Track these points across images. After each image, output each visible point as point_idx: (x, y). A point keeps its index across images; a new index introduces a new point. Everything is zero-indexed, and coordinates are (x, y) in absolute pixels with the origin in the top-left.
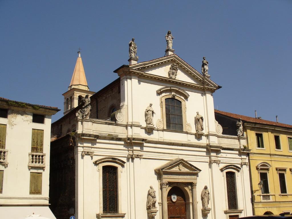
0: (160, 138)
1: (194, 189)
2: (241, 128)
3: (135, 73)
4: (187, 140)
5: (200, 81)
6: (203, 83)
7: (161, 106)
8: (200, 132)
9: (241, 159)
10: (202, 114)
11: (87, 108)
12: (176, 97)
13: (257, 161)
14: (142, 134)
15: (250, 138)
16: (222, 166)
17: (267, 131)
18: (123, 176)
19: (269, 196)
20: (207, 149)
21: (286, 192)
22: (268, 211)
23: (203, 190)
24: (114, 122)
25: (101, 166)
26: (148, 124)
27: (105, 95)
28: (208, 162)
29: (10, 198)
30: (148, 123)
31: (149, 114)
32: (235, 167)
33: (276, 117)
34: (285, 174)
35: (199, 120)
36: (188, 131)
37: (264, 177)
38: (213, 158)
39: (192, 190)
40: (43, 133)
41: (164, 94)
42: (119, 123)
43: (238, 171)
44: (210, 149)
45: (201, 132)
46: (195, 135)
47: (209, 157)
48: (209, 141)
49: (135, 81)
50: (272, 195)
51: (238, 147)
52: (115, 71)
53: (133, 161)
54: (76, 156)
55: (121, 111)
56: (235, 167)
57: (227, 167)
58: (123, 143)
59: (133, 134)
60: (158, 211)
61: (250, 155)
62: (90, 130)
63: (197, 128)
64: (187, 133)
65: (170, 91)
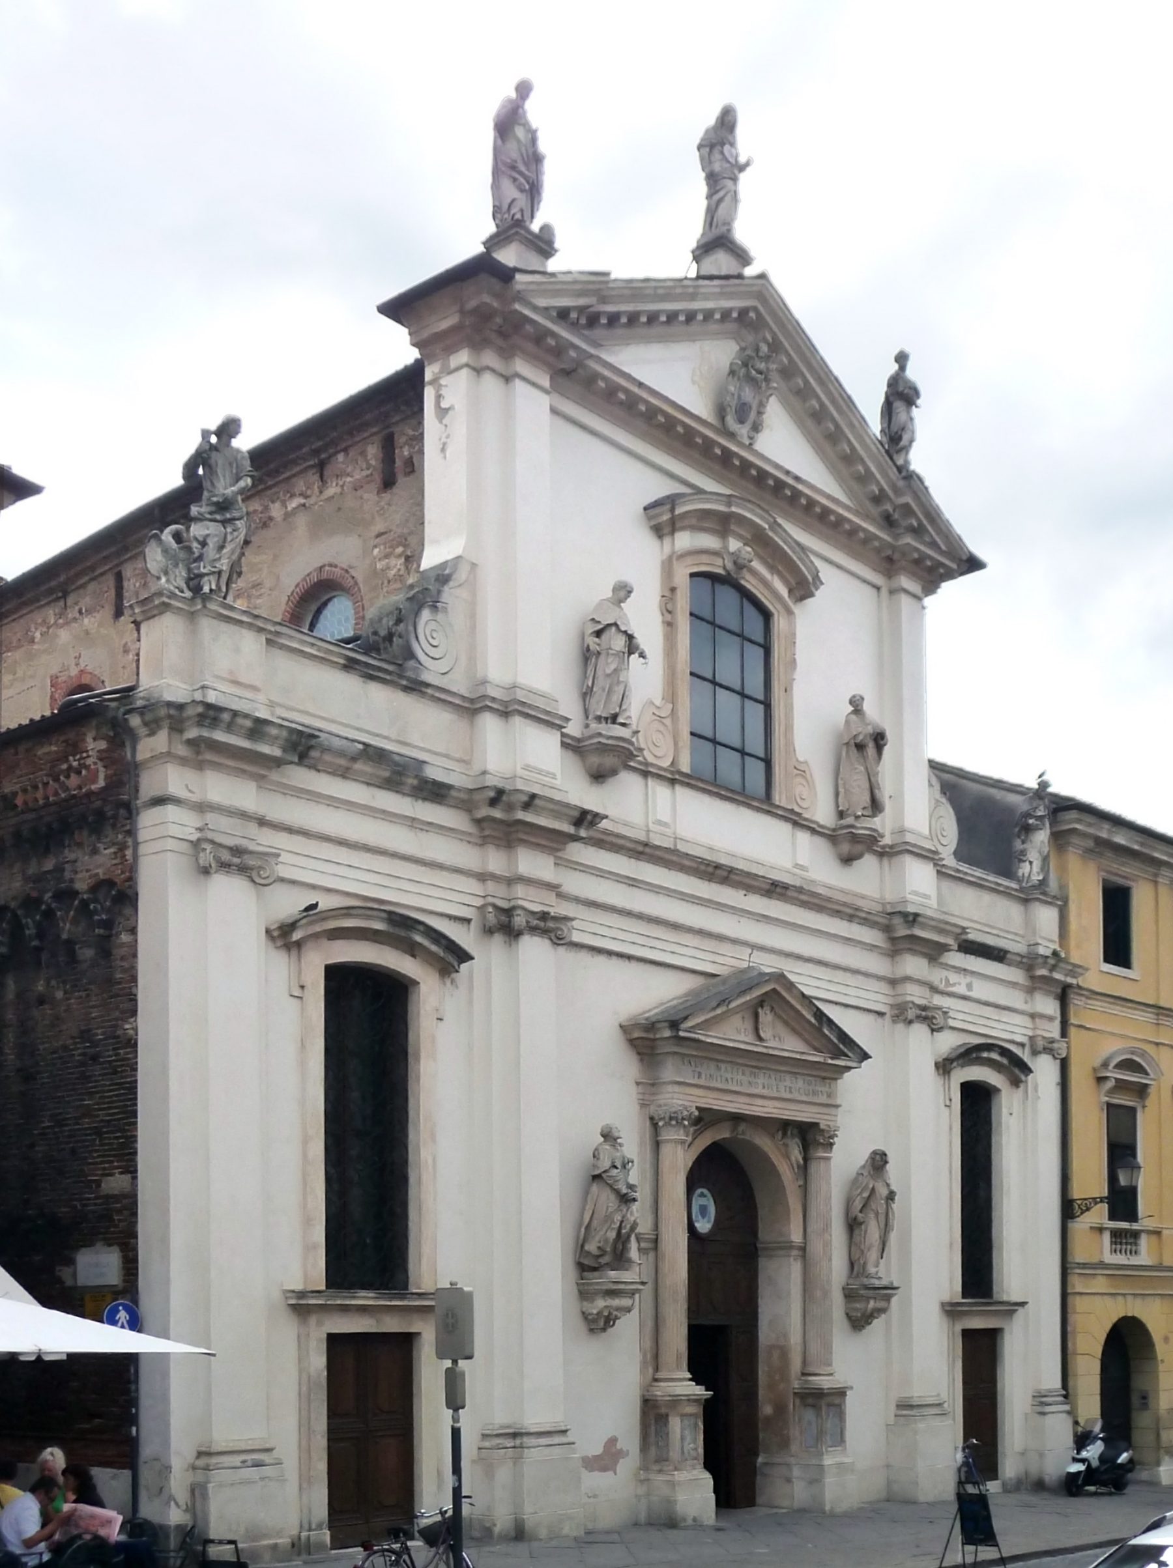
1: (813, 1167)
3: (540, 337)
4: (788, 865)
7: (668, 617)
8: (864, 826)
9: (1033, 1016)
11: (224, 522)
12: (748, 576)
13: (1104, 1036)
16: (948, 1042)
18: (448, 1041)
19: (1135, 1235)
21: (343, 983)
22: (1130, 1314)
23: (859, 1174)
26: (599, 719)
31: (600, 646)
32: (1005, 1061)
39: (804, 1170)
41: (684, 540)
43: (1016, 1083)
44: (903, 931)
49: (531, 404)
52: (396, 309)
60: (643, 1283)
61: (1076, 1001)
62: (249, 694)
64: (796, 820)
65: (722, 523)
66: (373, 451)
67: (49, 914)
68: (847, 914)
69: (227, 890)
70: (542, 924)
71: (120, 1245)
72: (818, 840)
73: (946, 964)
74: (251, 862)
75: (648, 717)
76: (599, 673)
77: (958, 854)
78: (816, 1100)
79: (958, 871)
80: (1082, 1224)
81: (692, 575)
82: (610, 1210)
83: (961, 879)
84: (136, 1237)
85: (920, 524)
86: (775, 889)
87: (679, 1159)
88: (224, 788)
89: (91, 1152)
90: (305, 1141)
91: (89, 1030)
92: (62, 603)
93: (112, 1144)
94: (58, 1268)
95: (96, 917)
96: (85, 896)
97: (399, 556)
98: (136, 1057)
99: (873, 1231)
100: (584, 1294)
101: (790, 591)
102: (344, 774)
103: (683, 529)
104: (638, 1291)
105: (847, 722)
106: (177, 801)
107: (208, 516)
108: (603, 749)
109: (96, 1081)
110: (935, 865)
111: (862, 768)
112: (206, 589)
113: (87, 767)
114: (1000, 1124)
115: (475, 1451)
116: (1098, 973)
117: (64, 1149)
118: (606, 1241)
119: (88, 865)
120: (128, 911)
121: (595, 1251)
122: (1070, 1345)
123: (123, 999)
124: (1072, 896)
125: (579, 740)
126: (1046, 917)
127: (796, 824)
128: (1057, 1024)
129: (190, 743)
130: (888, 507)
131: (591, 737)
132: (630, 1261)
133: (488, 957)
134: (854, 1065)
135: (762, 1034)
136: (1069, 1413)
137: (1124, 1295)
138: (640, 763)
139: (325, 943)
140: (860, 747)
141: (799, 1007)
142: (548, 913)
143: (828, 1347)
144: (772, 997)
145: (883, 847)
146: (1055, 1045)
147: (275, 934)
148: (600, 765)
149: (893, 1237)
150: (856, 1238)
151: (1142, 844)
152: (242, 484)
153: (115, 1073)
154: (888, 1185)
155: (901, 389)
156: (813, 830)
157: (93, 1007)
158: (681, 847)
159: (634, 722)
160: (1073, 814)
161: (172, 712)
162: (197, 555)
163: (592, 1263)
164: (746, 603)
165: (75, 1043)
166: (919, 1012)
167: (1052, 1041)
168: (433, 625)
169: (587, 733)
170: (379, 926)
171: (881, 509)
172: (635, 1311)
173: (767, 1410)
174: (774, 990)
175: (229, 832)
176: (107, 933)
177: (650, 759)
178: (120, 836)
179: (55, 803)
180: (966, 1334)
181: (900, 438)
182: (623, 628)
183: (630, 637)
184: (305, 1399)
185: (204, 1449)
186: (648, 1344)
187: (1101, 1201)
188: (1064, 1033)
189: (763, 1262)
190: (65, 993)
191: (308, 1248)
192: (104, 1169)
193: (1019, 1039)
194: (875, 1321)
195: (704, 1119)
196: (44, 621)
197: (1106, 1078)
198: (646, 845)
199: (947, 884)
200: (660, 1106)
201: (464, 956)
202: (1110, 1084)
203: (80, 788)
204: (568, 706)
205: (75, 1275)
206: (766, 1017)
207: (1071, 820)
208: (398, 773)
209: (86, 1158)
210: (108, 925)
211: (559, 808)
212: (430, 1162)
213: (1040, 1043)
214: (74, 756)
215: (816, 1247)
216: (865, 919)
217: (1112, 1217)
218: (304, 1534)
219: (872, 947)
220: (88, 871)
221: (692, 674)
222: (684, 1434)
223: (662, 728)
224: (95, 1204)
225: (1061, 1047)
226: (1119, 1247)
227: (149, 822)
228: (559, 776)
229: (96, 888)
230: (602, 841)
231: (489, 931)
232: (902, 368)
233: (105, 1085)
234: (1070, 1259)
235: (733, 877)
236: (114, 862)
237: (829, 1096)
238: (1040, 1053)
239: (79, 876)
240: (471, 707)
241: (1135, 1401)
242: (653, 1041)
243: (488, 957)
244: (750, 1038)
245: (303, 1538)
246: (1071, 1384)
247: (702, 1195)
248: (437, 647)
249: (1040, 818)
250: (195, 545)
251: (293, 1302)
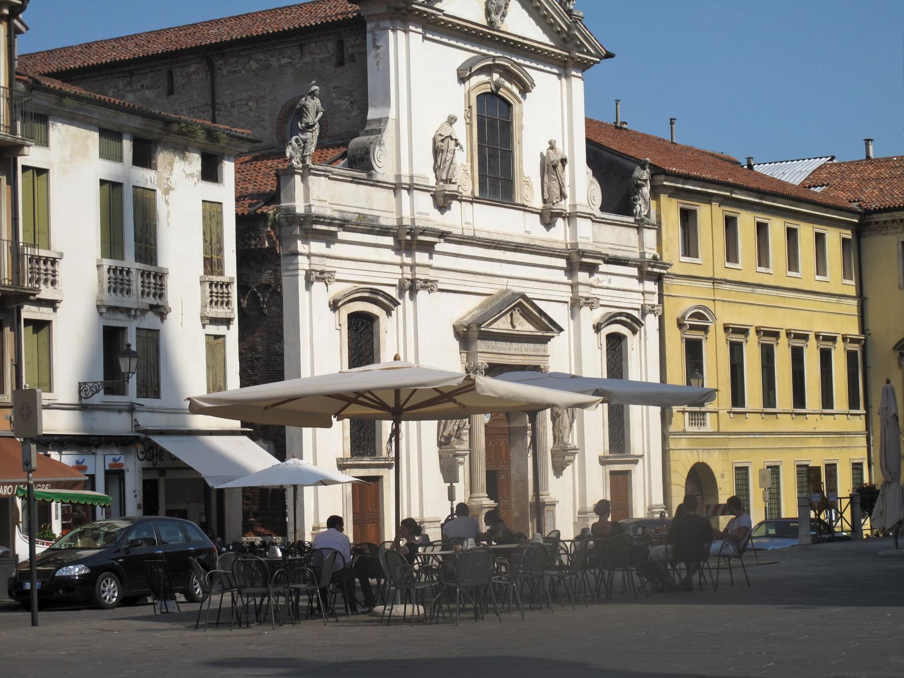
2: (646, 190)
4: (522, 232)
5: (558, 32)
6: (564, 40)
9: (643, 293)
10: (563, 149)
13: (684, 299)
14: (434, 219)
15: (667, 226)
16: (598, 314)
17: (708, 198)
19: (704, 413)
20: (568, 259)
21: (743, 405)
24: (364, 175)
26: (443, 180)
27: (261, 56)
28: (567, 302)
30: (444, 177)
32: (629, 321)
33: (672, 124)
35: (551, 167)
36: (526, 204)
37: (694, 351)
38: (583, 292)
40: (221, 212)
41: (475, 80)
42: (379, 177)
44: (578, 262)
46: (541, 215)
47: (572, 286)
48: (574, 233)
50: (711, 412)
51: (636, 255)
53: (413, 296)
54: (285, 280)
55: (384, 138)
56: (629, 321)
57: (612, 319)
58: (389, 241)
59: (416, 216)
61: (666, 281)
63: (546, 194)
64: (524, 208)
66: (331, 46)
74: (326, 275)
78: (538, 353)
88: (317, 247)
92: (129, 79)
97: (347, 100)
128: (656, 297)
158: (478, 235)
159: (458, 181)
167: (653, 306)
168: (380, 152)
188: (661, 301)
196: (115, 86)
204: (432, 182)
208: (368, 226)
249: (645, 181)
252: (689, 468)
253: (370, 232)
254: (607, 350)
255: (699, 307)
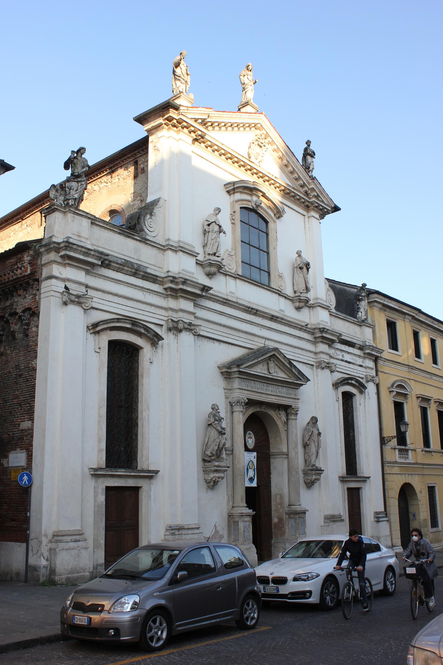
0: (230, 294)
4: (278, 310)
11: (78, 182)
12: (260, 209)
13: (390, 376)
16: (337, 376)
19: (407, 451)
21: (113, 345)
25: (105, 339)
29: (114, 252)
32: (357, 384)
34: (428, 409)
37: (399, 408)
39: (286, 423)
41: (238, 196)
43: (361, 392)
45: (305, 295)
57: (345, 381)
60: (228, 467)
61: (380, 362)
64: (280, 293)
67: (7, 322)
68: (299, 328)
69: (74, 311)
70: (189, 327)
71: (26, 449)
72: (288, 301)
73: (335, 348)
74: (82, 300)
75: (226, 255)
76: (209, 238)
77: (336, 308)
78: (290, 396)
79: (337, 314)
80: (387, 448)
81: (241, 208)
82: (215, 437)
83: (338, 317)
84: (32, 446)
85: (318, 195)
86: (273, 318)
87: (240, 419)
89: (17, 412)
90: (100, 408)
91: (19, 365)
93: (25, 409)
94: (2, 460)
95: (24, 322)
96: (21, 314)
98: (36, 375)
99: (313, 449)
100: (206, 471)
101: (275, 215)
102: (118, 270)
103: (237, 192)
104: (226, 470)
105: (296, 260)
106: (56, 278)
107: (72, 180)
108: (211, 265)
109: (20, 385)
110: (329, 311)
111: (302, 276)
112: (70, 204)
113: (24, 267)
114: (356, 408)
115: (163, 536)
116: (388, 353)
117: (7, 412)
118: (214, 450)
119: (22, 302)
120: (35, 319)
121: (210, 454)
122: (386, 494)
123: (31, 351)
124: (377, 325)
125: (202, 262)
126: (368, 331)
127: (279, 295)
129: (62, 257)
130: (306, 189)
131: (206, 261)
132: (223, 458)
133: (168, 338)
134: (304, 383)
135: (270, 371)
136: (387, 521)
137: (405, 474)
138: (224, 271)
139: (109, 332)
140: (301, 268)
141: (283, 361)
142: (192, 323)
143: (298, 494)
144: (271, 356)
145: (310, 304)
146: (374, 379)
147: (90, 328)
148: (209, 271)
149: (321, 451)
150: (307, 451)
151: (399, 307)
152: (84, 169)
153: (28, 381)
154: (318, 430)
155: (308, 152)
156: (286, 297)
157: (21, 356)
159: (222, 255)
160: (376, 295)
161: (56, 245)
162: (68, 192)
163: (208, 459)
164: (260, 219)
165: (13, 370)
166: (326, 365)
169: (205, 259)
170: (129, 326)
171: (304, 189)
172: (225, 479)
173: (275, 520)
174: (274, 354)
175: (75, 289)
176: (27, 328)
177: (227, 269)
178: (34, 292)
179: (12, 281)
180: (349, 489)
181: (309, 168)
182: (218, 223)
183: (220, 226)
184: (96, 513)
185: (55, 534)
186: (230, 493)
187: (395, 438)
188: (377, 375)
189: (272, 460)
190: (11, 351)
191: (100, 451)
192: (21, 419)
193: (361, 376)
194: (315, 484)
195: (250, 403)
197: (393, 391)
198: (227, 300)
199: (333, 319)
200: (233, 398)
201: (161, 338)
202: (394, 393)
203: (21, 274)
205: (8, 462)
206: (272, 364)
207: (374, 297)
208: (137, 271)
209: (15, 415)
210: (28, 324)
211: (195, 284)
212: (147, 417)
213: (369, 378)
214: (19, 263)
215: (292, 454)
216: (305, 330)
217: (399, 444)
218: (95, 571)
219: (308, 340)
220: (22, 305)
221: (242, 241)
222: (246, 527)
223: (231, 259)
224: (17, 433)
225: (377, 380)
226: (401, 456)
227: (45, 285)
228: (195, 274)
229: (24, 311)
230: (211, 298)
231: (170, 330)
232: (309, 146)
233: (24, 386)
234: (384, 460)
235: (258, 312)
236: (32, 301)
237: (295, 395)
238: (369, 381)
239: (19, 307)
240: (164, 248)
241: (411, 516)
242: (229, 371)
243: (168, 338)
244: (266, 372)
245: (94, 574)
246: (388, 510)
247: (250, 434)
248: (153, 227)
250: (67, 189)
251: (92, 473)
252: (400, 486)
253: (135, 274)
254: (343, 403)
255: (401, 381)
